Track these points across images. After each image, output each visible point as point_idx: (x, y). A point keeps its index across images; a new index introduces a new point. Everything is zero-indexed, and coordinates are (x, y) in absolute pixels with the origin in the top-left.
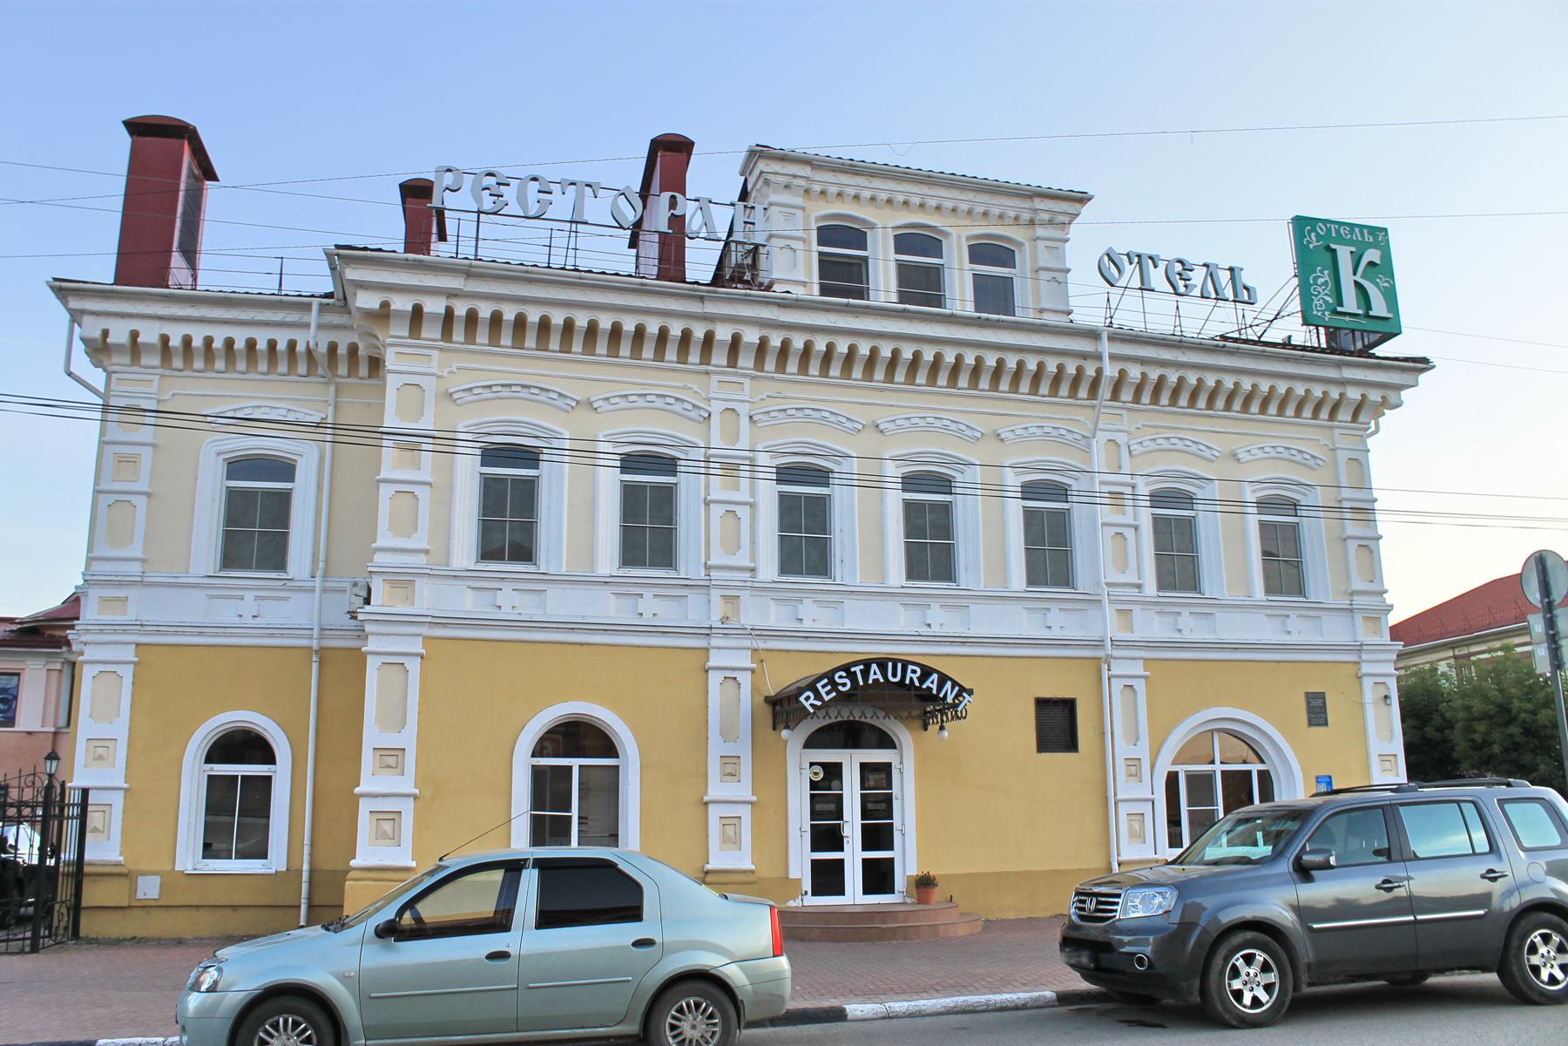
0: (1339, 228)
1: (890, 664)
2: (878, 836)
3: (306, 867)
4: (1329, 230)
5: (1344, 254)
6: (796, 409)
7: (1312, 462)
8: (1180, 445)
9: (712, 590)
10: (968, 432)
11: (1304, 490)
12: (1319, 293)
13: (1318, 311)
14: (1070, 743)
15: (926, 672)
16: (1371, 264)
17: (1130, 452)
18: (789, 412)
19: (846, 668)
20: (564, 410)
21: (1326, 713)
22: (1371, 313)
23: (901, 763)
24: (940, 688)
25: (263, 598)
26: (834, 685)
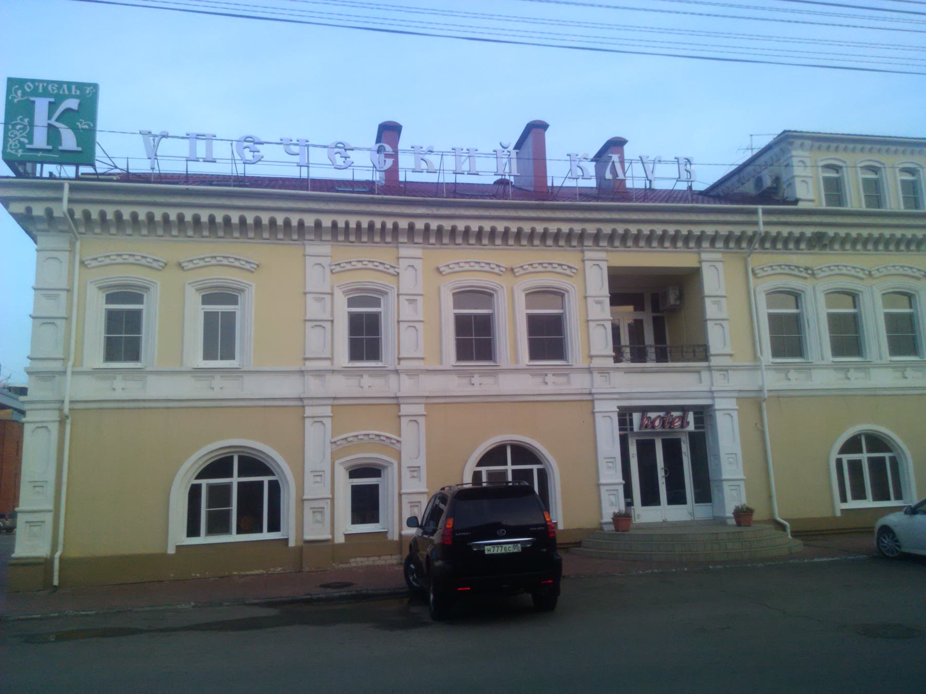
5: (41, 106)
7: (568, 272)
12: (16, 136)
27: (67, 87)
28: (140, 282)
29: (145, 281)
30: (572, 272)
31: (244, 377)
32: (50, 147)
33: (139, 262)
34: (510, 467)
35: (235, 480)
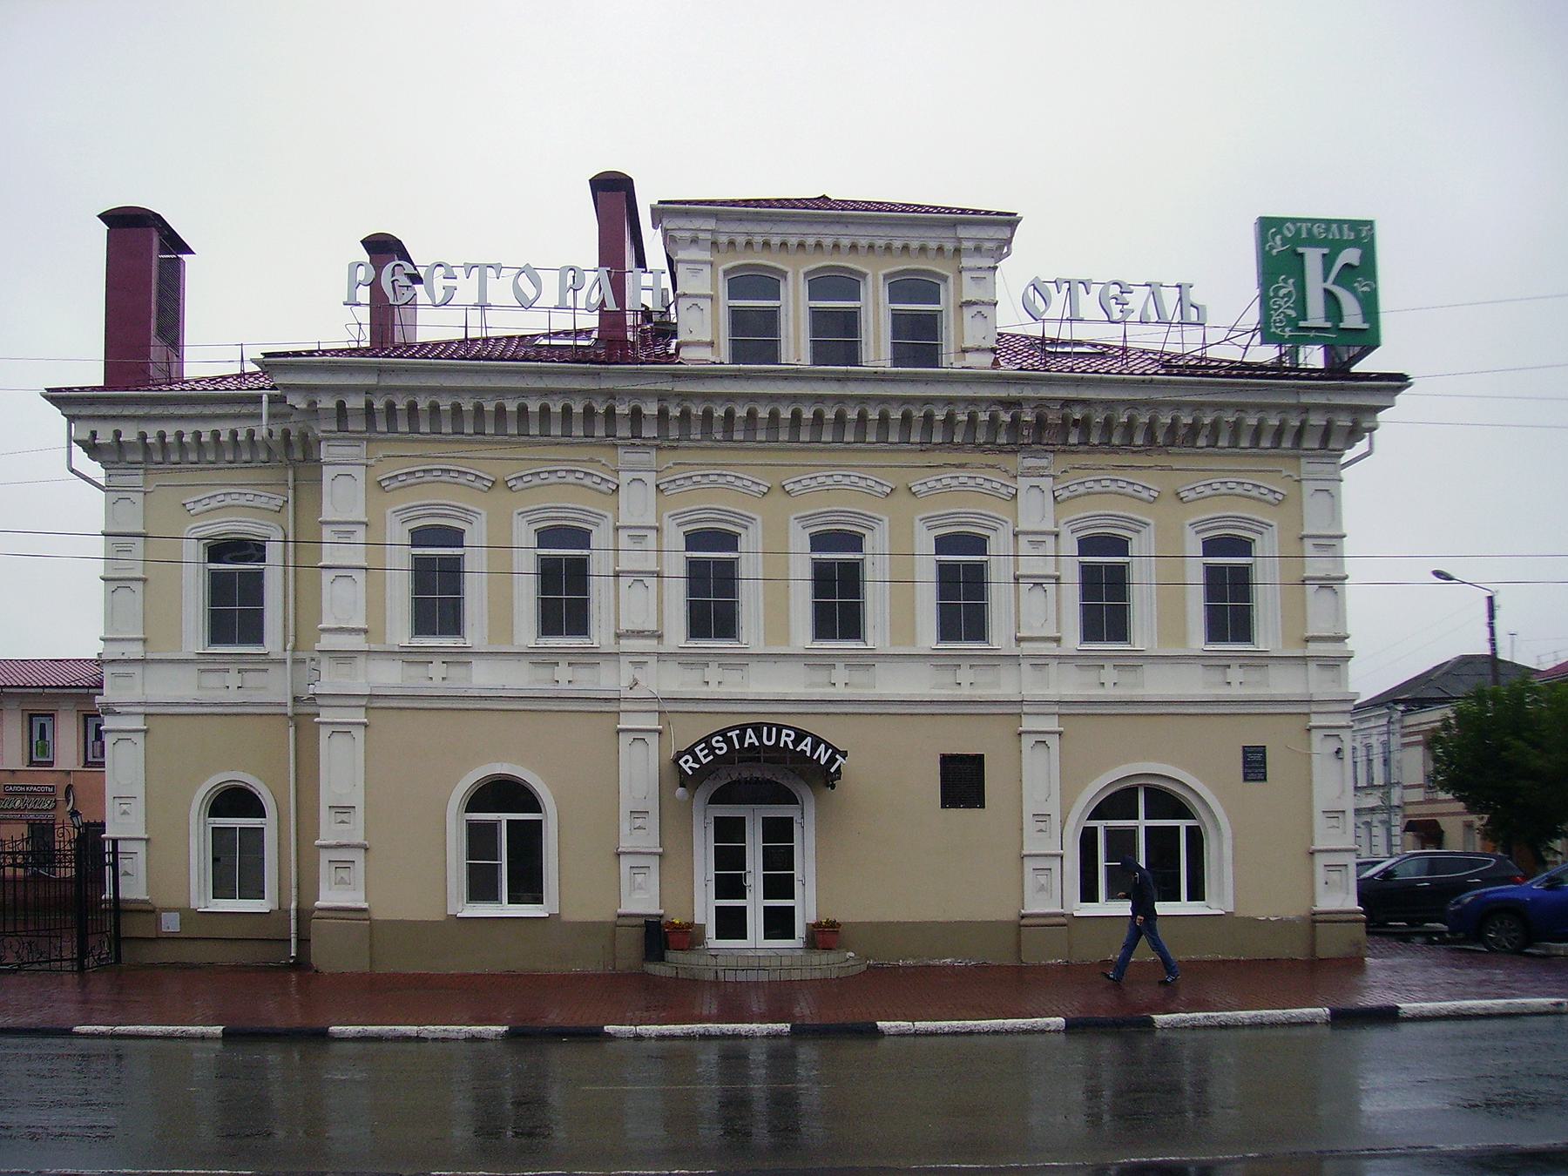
1: (765, 728)
2: (779, 885)
3: (293, 905)
4: (1298, 231)
5: (1313, 258)
6: (702, 475)
8: (1113, 487)
9: (621, 657)
10: (878, 488)
13: (1277, 327)
15: (800, 736)
17: (1055, 498)
18: (695, 479)
19: (723, 733)
20: (482, 490)
21: (1265, 768)
22: (1342, 325)
23: (803, 818)
24: (814, 750)
25: (246, 671)
26: (712, 749)
27: (1338, 227)
29: (850, 515)
31: (1342, 666)
32: (1328, 325)
33: (1109, 489)
34: (1142, 823)
35: (1142, 823)
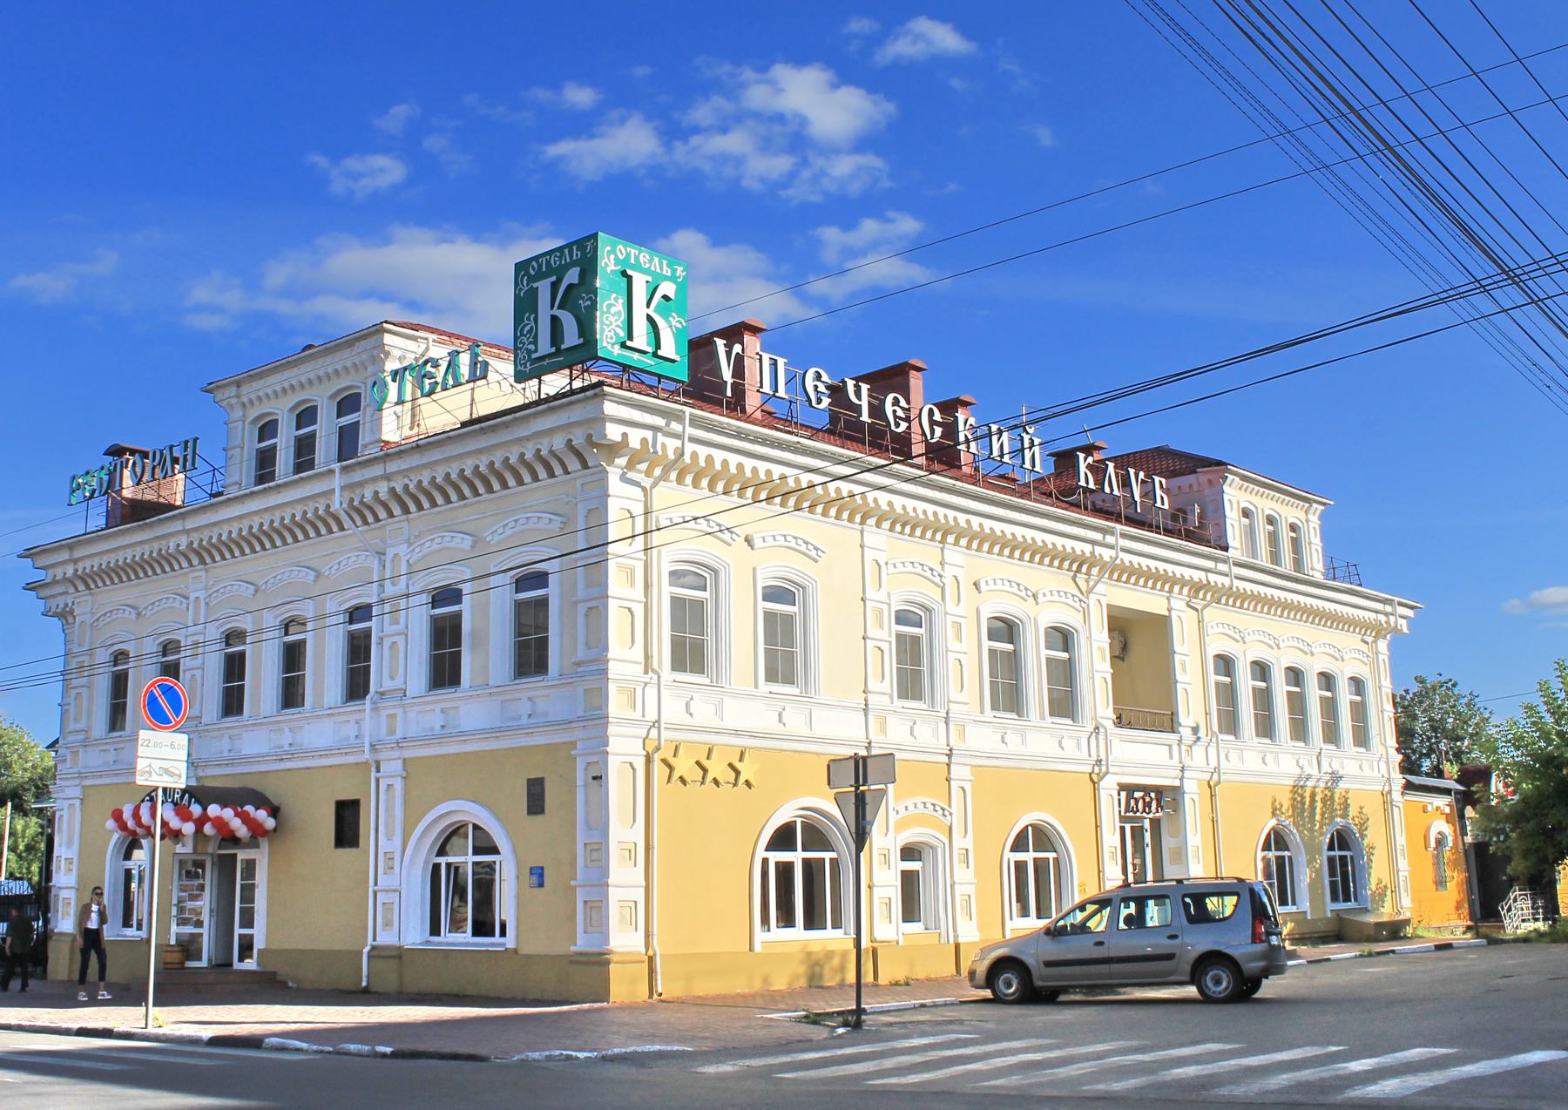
0: (639, 254)
11: (532, 549)
12: (611, 323)
13: (608, 343)
14: (698, 666)
16: (666, 298)
28: (708, 558)
30: (1081, 606)
